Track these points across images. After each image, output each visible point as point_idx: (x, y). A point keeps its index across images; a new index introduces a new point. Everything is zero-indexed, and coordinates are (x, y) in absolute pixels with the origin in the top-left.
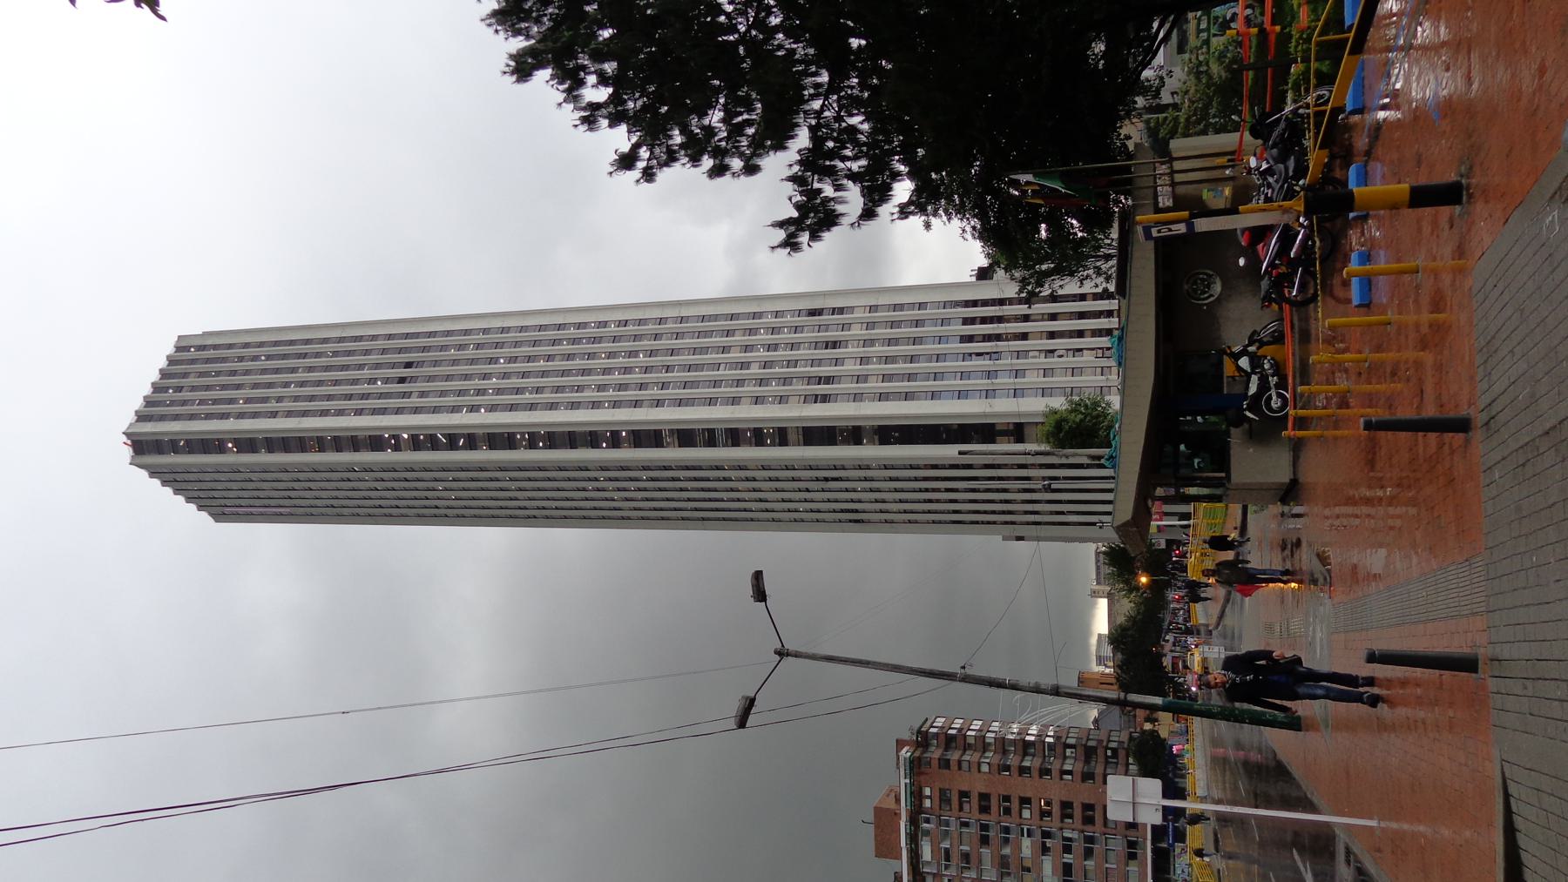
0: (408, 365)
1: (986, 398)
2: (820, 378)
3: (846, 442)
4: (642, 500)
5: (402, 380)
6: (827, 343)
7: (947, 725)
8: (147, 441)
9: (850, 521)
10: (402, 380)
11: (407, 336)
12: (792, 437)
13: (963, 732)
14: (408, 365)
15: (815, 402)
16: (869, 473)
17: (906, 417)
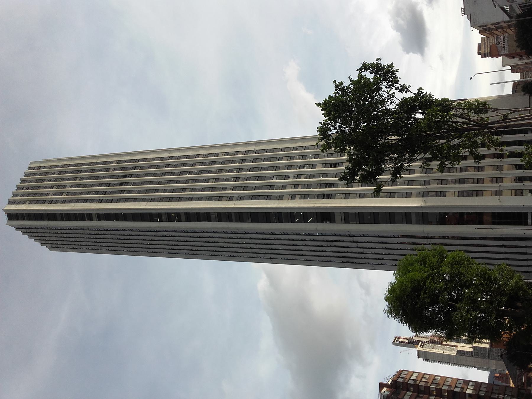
0: (125, 176)
1: (458, 196)
2: (327, 184)
3: (287, 221)
4: (48, 237)
5: (121, 184)
6: (331, 164)
7: (408, 377)
8: (352, 214)
9: (349, 262)
10: (121, 184)
11: (126, 161)
12: (414, 218)
13: (418, 383)
14: (125, 176)
15: (323, 198)
16: (356, 239)
17: (514, 207)
